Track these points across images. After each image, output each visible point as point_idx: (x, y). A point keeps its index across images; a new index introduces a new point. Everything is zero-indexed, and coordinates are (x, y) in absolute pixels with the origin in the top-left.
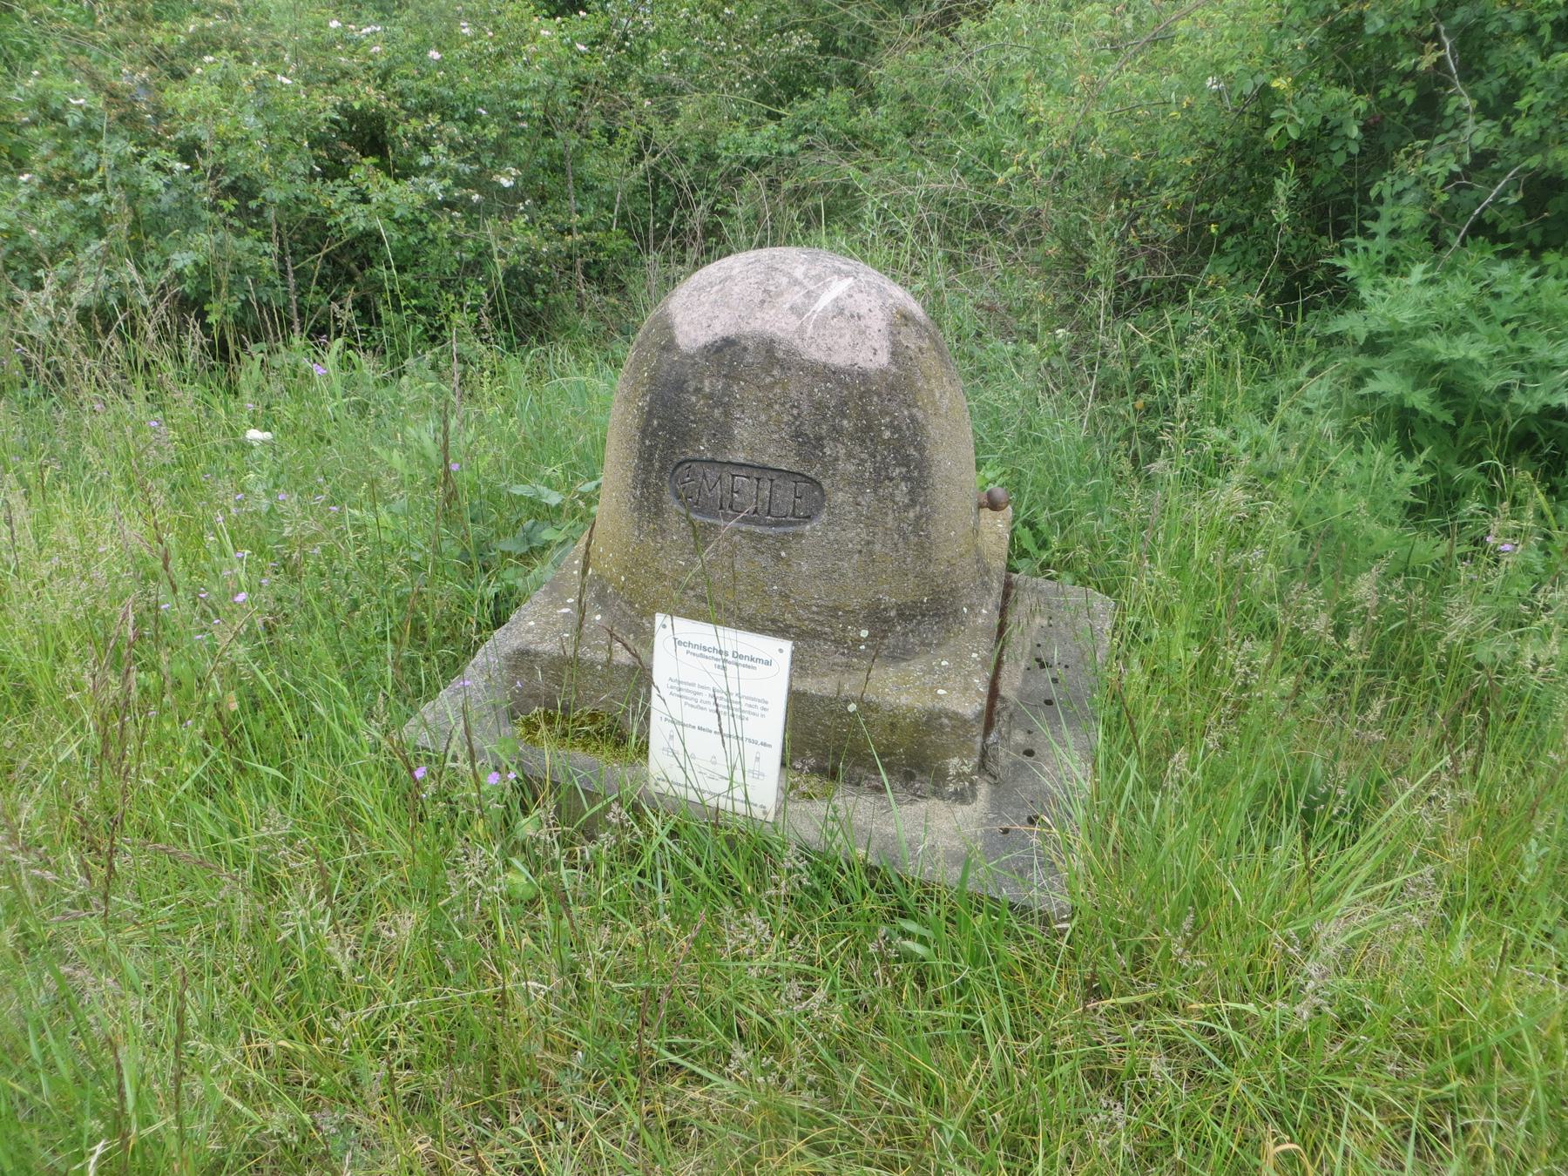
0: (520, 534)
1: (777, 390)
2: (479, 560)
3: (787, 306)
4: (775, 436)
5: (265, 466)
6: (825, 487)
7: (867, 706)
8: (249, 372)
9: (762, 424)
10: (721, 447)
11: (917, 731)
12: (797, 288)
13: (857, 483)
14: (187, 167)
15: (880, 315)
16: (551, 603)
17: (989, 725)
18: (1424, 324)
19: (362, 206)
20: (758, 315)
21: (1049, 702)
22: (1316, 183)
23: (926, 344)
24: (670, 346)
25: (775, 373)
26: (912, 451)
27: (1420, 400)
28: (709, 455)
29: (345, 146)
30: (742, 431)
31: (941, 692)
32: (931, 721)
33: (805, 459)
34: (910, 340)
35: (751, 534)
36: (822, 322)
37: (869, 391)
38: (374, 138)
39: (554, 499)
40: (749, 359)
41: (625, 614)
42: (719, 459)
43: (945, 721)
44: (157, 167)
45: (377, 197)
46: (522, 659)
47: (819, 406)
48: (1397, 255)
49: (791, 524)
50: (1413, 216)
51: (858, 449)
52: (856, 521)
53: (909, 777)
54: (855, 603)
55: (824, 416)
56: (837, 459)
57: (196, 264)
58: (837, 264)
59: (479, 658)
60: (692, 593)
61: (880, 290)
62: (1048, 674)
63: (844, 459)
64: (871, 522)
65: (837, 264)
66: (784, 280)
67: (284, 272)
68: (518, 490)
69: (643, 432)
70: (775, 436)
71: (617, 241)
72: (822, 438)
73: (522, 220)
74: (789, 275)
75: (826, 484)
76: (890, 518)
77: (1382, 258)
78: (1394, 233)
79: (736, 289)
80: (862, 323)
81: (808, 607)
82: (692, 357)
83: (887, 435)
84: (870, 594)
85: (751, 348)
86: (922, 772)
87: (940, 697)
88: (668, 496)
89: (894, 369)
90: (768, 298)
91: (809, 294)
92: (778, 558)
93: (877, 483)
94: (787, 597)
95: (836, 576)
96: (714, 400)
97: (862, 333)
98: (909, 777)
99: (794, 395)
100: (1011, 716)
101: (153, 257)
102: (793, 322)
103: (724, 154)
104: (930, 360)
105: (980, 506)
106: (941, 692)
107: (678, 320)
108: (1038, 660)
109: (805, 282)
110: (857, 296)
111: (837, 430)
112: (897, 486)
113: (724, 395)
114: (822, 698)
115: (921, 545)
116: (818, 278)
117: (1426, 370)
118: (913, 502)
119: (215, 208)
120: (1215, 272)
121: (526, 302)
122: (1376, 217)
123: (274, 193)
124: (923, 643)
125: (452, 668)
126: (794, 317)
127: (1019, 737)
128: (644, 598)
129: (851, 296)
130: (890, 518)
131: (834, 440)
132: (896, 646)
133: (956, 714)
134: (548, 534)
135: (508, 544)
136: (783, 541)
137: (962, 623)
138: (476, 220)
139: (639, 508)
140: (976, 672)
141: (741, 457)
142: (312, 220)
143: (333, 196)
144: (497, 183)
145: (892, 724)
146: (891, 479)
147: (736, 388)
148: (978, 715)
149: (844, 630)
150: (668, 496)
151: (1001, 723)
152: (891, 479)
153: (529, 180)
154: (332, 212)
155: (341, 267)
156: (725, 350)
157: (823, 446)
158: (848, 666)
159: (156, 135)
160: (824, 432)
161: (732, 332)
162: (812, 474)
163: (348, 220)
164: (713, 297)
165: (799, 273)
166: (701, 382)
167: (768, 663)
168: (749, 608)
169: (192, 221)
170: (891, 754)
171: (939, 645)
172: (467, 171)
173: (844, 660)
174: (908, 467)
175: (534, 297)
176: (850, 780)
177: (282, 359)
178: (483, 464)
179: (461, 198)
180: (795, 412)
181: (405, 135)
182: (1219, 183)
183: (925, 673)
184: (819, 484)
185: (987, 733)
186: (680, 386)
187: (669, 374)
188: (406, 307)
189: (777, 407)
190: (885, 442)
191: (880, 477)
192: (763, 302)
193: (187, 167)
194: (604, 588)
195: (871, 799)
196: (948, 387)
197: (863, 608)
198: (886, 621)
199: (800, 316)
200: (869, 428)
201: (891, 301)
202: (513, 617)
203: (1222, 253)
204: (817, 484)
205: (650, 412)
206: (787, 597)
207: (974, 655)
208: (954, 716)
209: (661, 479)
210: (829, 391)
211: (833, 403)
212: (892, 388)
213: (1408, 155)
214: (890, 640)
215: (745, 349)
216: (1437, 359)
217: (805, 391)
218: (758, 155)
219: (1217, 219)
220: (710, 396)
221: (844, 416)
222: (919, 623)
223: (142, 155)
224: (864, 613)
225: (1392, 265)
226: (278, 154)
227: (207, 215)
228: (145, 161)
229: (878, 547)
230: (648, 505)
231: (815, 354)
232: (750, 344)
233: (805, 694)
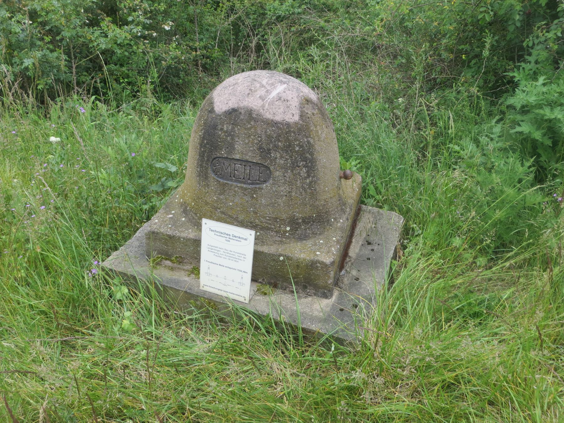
0: (160, 183)
1: (252, 130)
2: (142, 192)
3: (258, 96)
4: (251, 149)
5: (57, 152)
6: (271, 169)
7: (288, 258)
8: (54, 109)
9: (246, 143)
10: (230, 152)
11: (307, 268)
12: (263, 89)
13: (284, 168)
14: (31, 22)
15: (296, 100)
16: (165, 212)
17: (341, 267)
18: (540, 102)
19: (105, 39)
20: (246, 99)
21: (369, 259)
22: (508, 38)
23: (316, 112)
24: (212, 111)
25: (252, 123)
26: (308, 155)
27: (537, 135)
28: (225, 155)
29: (99, 12)
30: (238, 147)
31: (318, 253)
32: (313, 265)
33: (264, 158)
34: (309, 110)
35: (242, 187)
36: (272, 103)
37: (290, 131)
38: (112, 8)
39: (173, 169)
40: (242, 117)
41: (193, 218)
42: (229, 157)
43: (319, 265)
44: (18, 22)
45: (110, 35)
46: (153, 235)
47: (269, 137)
48: (537, 71)
49: (258, 184)
50: (544, 55)
51: (285, 154)
52: (284, 183)
53: (305, 287)
54: (284, 216)
55: (271, 141)
56: (276, 158)
57: (34, 64)
58: (281, 78)
59: (137, 234)
60: (219, 211)
61: (298, 89)
62: (370, 247)
64: (290, 183)
65: (281, 78)
66: (258, 85)
67: (70, 68)
68: (158, 165)
69: (201, 145)
70: (251, 149)
71: (216, 53)
72: (270, 150)
73: (174, 45)
74: (260, 83)
75: (272, 168)
76: (298, 182)
77: (531, 72)
78: (537, 62)
79: (239, 88)
80: (288, 103)
81: (265, 217)
82: (220, 116)
83: (297, 149)
84: (291, 213)
85: (243, 113)
86: (310, 285)
87: (317, 255)
88: (210, 171)
89: (301, 122)
90: (251, 92)
91: (267, 91)
92: (253, 197)
93: (293, 168)
94: (256, 213)
95: (276, 205)
96: (228, 133)
97: (288, 107)
98: (305, 287)
99: (259, 132)
100: (352, 264)
101: (16, 60)
102: (260, 103)
103: (269, 13)
104: (317, 118)
105: (341, 178)
106: (318, 253)
107: (215, 100)
108: (367, 241)
109: (267, 86)
110: (287, 92)
111: (276, 147)
112: (301, 170)
113: (232, 132)
114: (270, 254)
115: (312, 193)
116: (272, 84)
117: (539, 122)
118: (309, 176)
119: (42, 39)
120: (466, 75)
121: (175, 80)
122: (530, 54)
123: (66, 34)
124: (313, 233)
125: (126, 238)
126: (261, 101)
127: (354, 273)
128: (201, 212)
129: (284, 92)
130: (298, 182)
131: (275, 150)
133: (323, 262)
134: (171, 184)
135: (154, 187)
136: (255, 191)
137: (331, 225)
138: (155, 44)
139: (199, 176)
140: (334, 246)
141: (237, 157)
142: (84, 44)
143: (92, 34)
144: (164, 28)
145: (297, 265)
146: (299, 167)
147: (236, 129)
148: (333, 263)
150: (210, 171)
151: (347, 267)
152: (299, 167)
153: (177, 26)
154: (92, 41)
155: (97, 63)
156: (233, 113)
157: (270, 153)
158: (281, 241)
159: (19, 8)
160: (271, 147)
161: (236, 106)
162: (266, 164)
163: (98, 45)
164: (229, 91)
165: (264, 82)
166: (223, 126)
167: (246, 239)
168: (241, 217)
169: (33, 45)
170: (298, 278)
171: (320, 234)
172: (148, 22)
173: (280, 239)
174: (306, 162)
175: (179, 78)
176: (282, 288)
177: (70, 103)
178: (145, 154)
179: (148, 34)
180: (259, 139)
181: (125, 6)
182: (469, 37)
183: (313, 245)
184: (269, 168)
185: (341, 269)
186: (215, 127)
187: (211, 122)
188: (123, 82)
189: (252, 137)
190: (296, 152)
191: (294, 166)
192: (249, 94)
193: (31, 22)
194: (186, 207)
195: (290, 296)
196: (325, 129)
198: (297, 224)
199: (263, 100)
200: (290, 146)
201: (302, 94)
202: (152, 218)
203: (469, 67)
204: (268, 168)
205: (203, 137)
206: (256, 213)
207: (334, 239)
208: (322, 263)
209: (207, 164)
210: (273, 131)
211: (275, 136)
212: (300, 129)
213: (539, 28)
214: (299, 232)
215: (240, 113)
216: (546, 118)
217: (264, 131)
218: (283, 14)
219: (466, 53)
220: (226, 132)
221: (279, 141)
222: (312, 225)
223: (12, 17)
225: (534, 76)
226: (68, 18)
227: (39, 43)
228: (13, 20)
229: (293, 194)
230: (202, 175)
231: (268, 116)
232: (243, 112)
233: (263, 252)
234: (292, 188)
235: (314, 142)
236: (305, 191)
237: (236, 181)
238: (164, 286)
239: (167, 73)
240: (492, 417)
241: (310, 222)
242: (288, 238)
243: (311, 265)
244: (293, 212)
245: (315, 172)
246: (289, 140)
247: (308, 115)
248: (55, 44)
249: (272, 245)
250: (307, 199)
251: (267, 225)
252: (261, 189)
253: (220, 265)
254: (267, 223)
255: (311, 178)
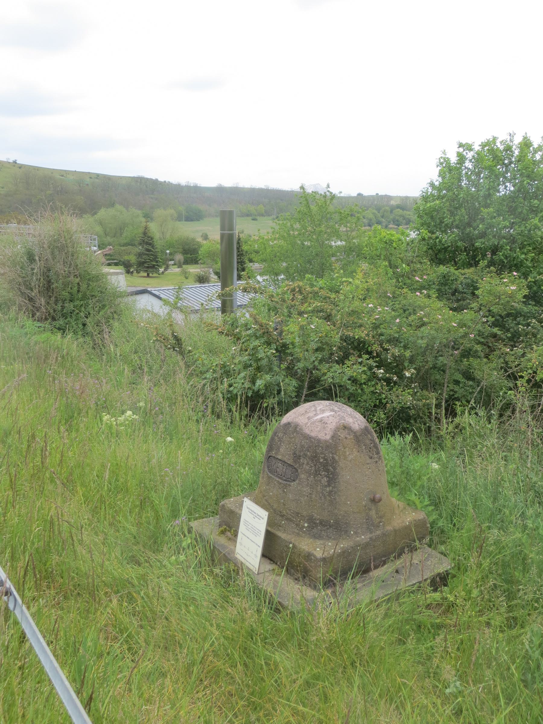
7: (294, 546)
10: (276, 453)
32: (308, 556)
33: (295, 462)
35: (278, 481)
36: (313, 423)
37: (319, 445)
43: (313, 558)
47: (302, 446)
49: (289, 481)
54: (305, 513)
56: (304, 464)
63: (306, 465)
75: (299, 470)
76: (319, 487)
81: (290, 510)
83: (322, 460)
84: (310, 512)
89: (331, 441)
95: (299, 502)
97: (324, 428)
111: (306, 455)
114: (284, 540)
118: (329, 485)
124: (327, 536)
130: (319, 487)
132: (317, 534)
137: (349, 536)
141: (280, 457)
146: (321, 475)
149: (300, 521)
152: (321, 475)
157: (300, 459)
162: (296, 466)
173: (297, 531)
174: (328, 473)
190: (320, 462)
191: (317, 473)
197: (307, 516)
198: (315, 523)
204: (297, 471)
214: (315, 530)
221: (308, 451)
222: (328, 529)
224: (307, 518)
231: (307, 431)
234: (313, 491)
235: (339, 459)
236: (325, 498)
237: (277, 476)
238: (214, 547)
239: (398, 417)
240: (12, 425)
241: (326, 526)
242: (304, 532)
243: (308, 556)
244: (312, 512)
245: (337, 484)
246: (316, 452)
247: (340, 438)
248: (290, 371)
249: (290, 534)
250: (326, 505)
251: (290, 517)
252: (290, 485)
253: (257, 544)
254: (291, 515)
255: (331, 488)
